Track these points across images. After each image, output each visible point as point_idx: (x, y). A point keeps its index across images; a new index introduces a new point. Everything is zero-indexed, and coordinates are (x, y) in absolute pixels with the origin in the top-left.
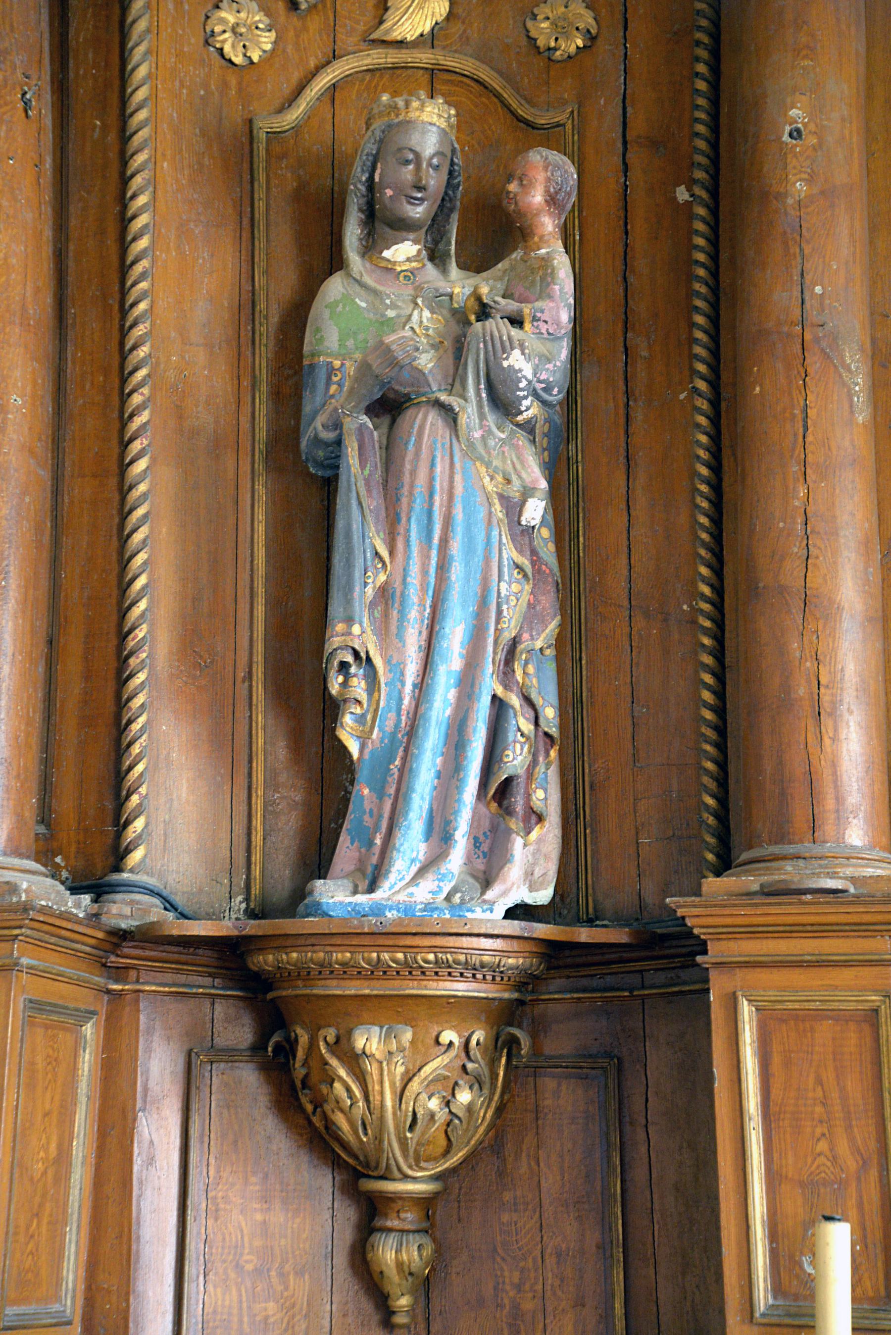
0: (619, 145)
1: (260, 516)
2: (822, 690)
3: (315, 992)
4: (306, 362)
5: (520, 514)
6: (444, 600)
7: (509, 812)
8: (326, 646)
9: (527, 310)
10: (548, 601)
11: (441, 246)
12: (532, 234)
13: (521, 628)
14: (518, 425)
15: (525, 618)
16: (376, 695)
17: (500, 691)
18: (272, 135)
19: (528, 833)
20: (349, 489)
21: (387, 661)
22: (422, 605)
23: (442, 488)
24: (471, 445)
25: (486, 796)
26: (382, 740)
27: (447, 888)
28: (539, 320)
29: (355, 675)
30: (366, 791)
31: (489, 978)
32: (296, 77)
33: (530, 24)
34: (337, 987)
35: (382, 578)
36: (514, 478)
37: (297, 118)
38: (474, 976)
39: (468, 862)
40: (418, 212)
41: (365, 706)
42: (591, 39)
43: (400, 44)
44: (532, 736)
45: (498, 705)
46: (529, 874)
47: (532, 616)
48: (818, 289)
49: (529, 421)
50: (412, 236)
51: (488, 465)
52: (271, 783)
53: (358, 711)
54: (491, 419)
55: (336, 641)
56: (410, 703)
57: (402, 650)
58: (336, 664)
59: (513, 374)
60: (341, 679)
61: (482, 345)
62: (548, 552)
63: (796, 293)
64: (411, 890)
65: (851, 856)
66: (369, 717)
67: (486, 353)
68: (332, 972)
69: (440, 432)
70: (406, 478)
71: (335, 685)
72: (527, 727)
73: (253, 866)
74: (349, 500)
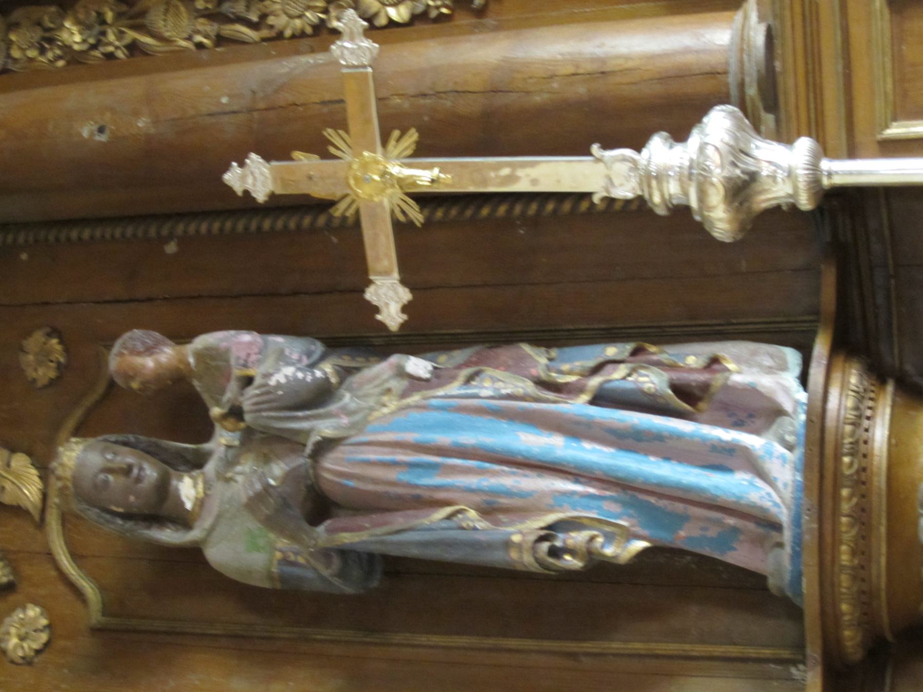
0: (133, 305)
1: (423, 639)
2: (581, 71)
3: (883, 585)
4: (278, 586)
5: (420, 379)
6: (493, 450)
7: (705, 387)
8: (533, 570)
9: (237, 372)
10: (505, 353)
11: (189, 457)
12: (178, 369)
13: (526, 377)
14: (341, 382)
15: (516, 373)
16: (585, 522)
17: (585, 397)
18: (105, 612)
19: (728, 370)
20: (382, 543)
21: (550, 510)
22: (495, 474)
23: (389, 454)
24: (353, 426)
25: (692, 413)
26: (630, 516)
27: (780, 449)
28: (246, 361)
29: (564, 542)
30: (682, 533)
31: (871, 403)
32: (62, 588)
33: (40, 384)
34: (878, 563)
35: (472, 513)
36: (387, 385)
37: (92, 589)
38: (868, 418)
39: (757, 432)
40: (151, 472)
41: (595, 533)
42: (55, 332)
43: (45, 496)
44: (630, 365)
45: (601, 399)
46: (770, 370)
47: (518, 368)
48: (224, 100)
49: (338, 373)
50: (174, 482)
51: (372, 409)
52: (681, 636)
53: (600, 540)
54: (333, 407)
55: (527, 560)
56: (593, 487)
57: (543, 494)
58: (551, 560)
59: (293, 385)
60: (567, 557)
61: (264, 414)
62: (460, 355)
63: (226, 119)
64: (780, 485)
65: (742, 39)
66: (608, 529)
67: (270, 409)
68: (863, 567)
69: (340, 455)
70: (380, 488)
71: (570, 562)
72: (622, 370)
73: (761, 656)
74: (392, 543)
